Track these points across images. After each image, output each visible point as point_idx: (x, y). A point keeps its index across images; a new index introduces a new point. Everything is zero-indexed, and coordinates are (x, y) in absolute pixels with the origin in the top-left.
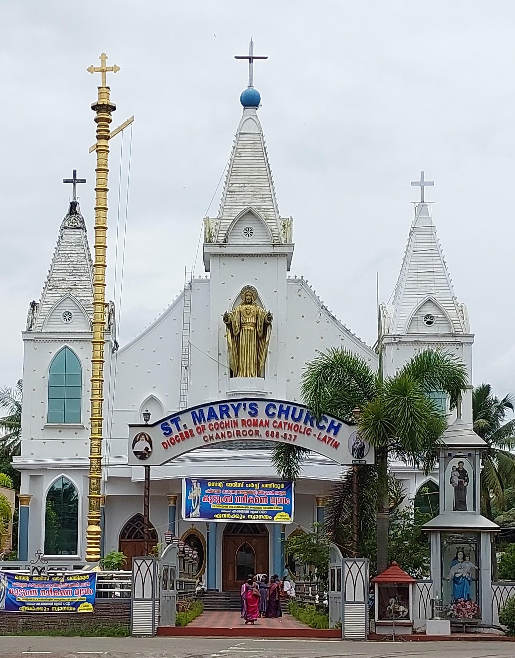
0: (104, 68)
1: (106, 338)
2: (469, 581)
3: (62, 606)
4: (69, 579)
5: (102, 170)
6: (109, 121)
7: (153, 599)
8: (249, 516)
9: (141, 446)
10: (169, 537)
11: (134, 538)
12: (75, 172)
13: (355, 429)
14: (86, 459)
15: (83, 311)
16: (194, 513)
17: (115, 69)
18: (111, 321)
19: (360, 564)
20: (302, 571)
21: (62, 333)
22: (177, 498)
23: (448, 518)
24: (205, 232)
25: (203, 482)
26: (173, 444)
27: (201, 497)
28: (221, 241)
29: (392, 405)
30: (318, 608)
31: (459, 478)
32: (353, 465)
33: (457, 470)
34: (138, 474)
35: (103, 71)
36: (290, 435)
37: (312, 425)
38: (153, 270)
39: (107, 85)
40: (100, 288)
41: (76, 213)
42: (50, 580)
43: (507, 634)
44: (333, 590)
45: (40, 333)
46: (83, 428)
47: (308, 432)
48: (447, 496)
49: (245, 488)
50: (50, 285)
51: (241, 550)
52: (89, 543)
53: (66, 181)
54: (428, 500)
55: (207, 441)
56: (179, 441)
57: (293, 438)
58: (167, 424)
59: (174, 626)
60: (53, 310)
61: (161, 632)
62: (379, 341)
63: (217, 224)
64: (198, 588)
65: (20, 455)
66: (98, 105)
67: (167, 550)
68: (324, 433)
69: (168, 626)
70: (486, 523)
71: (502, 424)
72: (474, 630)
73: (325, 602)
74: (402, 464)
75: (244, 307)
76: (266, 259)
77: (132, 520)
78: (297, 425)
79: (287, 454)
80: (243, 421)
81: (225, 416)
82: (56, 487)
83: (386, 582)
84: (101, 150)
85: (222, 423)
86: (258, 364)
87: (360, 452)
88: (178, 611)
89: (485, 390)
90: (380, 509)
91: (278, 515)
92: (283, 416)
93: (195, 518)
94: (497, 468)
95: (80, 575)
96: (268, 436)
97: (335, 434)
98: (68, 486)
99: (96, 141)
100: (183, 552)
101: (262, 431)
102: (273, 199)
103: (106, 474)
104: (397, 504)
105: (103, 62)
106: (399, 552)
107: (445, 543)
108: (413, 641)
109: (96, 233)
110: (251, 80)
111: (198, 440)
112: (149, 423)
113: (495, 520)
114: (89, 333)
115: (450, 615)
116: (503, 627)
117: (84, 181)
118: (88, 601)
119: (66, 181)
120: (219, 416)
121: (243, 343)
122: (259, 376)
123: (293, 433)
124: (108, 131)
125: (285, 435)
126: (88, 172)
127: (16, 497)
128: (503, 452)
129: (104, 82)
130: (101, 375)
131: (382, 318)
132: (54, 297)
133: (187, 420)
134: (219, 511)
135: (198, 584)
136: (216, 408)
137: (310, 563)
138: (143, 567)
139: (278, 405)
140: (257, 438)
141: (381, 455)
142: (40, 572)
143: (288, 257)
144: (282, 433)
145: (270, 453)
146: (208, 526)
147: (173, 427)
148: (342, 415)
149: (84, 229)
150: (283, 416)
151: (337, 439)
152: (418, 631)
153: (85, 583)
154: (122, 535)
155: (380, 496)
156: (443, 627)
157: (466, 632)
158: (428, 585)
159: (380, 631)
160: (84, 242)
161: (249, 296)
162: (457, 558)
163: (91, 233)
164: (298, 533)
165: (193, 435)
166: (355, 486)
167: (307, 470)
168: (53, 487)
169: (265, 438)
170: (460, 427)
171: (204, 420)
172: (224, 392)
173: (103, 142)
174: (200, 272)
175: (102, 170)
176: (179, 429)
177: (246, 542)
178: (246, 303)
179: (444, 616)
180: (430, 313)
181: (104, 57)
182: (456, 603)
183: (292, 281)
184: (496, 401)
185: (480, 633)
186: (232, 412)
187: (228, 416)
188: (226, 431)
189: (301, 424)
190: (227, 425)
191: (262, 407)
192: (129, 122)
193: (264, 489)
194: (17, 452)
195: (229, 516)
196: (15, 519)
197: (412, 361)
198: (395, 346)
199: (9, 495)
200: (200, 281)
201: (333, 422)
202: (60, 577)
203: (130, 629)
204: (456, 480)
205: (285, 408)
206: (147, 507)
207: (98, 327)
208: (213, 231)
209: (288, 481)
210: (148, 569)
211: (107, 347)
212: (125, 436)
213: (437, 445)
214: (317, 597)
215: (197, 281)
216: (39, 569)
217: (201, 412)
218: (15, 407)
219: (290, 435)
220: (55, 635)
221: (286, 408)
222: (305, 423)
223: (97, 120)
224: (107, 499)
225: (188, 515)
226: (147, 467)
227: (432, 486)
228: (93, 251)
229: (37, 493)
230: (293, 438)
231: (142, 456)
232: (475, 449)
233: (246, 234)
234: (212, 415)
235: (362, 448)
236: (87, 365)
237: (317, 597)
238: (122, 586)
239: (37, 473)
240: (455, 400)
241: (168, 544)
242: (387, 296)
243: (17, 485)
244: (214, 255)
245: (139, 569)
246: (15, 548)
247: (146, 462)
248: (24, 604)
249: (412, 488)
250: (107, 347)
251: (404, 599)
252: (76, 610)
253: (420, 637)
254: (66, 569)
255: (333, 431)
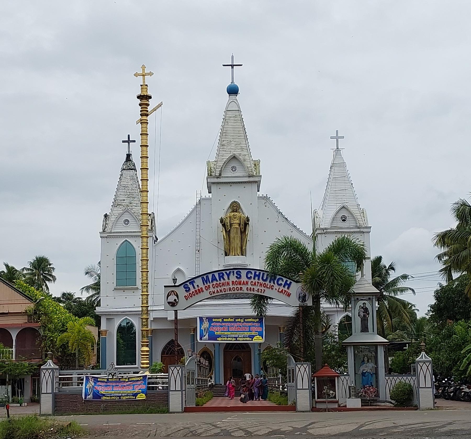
0: (144, 74)
1: (150, 234)
2: (372, 375)
3: (127, 396)
4: (130, 380)
5: (144, 134)
6: (148, 105)
7: (181, 390)
8: (238, 339)
9: (172, 298)
10: (190, 353)
11: (170, 354)
12: (129, 136)
13: (300, 285)
14: (138, 307)
15: (135, 218)
16: (205, 338)
17: (151, 74)
18: (153, 224)
19: (305, 366)
20: (271, 372)
21: (124, 232)
22: (195, 330)
23: (358, 337)
24: (208, 170)
25: (210, 319)
26: (191, 297)
27: (209, 327)
28: (217, 174)
29: (321, 269)
30: (282, 393)
31: (363, 312)
32: (299, 307)
33: (362, 308)
34: (171, 317)
35: (143, 75)
36: (261, 290)
37: (274, 283)
38: (178, 194)
39: (146, 84)
40: (145, 205)
41: (130, 161)
42: (119, 380)
43: (395, 406)
44: (290, 382)
45: (111, 233)
46: (137, 289)
47: (272, 288)
48: (357, 323)
49: (235, 322)
50: (116, 204)
51: (235, 359)
52: (142, 358)
53: (124, 142)
54: (346, 326)
55: (211, 294)
56: (194, 295)
57: (263, 291)
58: (187, 285)
59: (194, 406)
60: (118, 219)
61: (187, 410)
62: (314, 233)
63: (215, 165)
64: (210, 383)
65: (100, 306)
66: (141, 96)
67: (190, 361)
68: (282, 288)
69: (191, 406)
70: (381, 339)
71: (390, 280)
72: (375, 404)
73: (286, 390)
74: (329, 305)
75: (232, 214)
76: (245, 185)
77: (169, 343)
78: (265, 284)
79: (260, 301)
80: (233, 282)
81: (222, 279)
82: (122, 325)
83: (323, 377)
84: (144, 123)
85: (220, 283)
86: (241, 248)
87: (303, 298)
88: (197, 397)
89: (379, 259)
90: (317, 333)
91: (255, 338)
92: (257, 278)
93: (206, 339)
94: (388, 306)
95: (137, 377)
96: (248, 290)
97: (288, 288)
98: (129, 324)
99: (140, 117)
100: (200, 361)
101: (244, 288)
102: (248, 149)
103: (152, 316)
104: (327, 329)
105: (143, 70)
106: (329, 358)
107: (356, 352)
108: (339, 411)
109: (142, 172)
110: (233, 78)
111: (206, 294)
112: (176, 284)
113: (388, 338)
114: (139, 232)
115: (361, 396)
116: (393, 401)
117: (134, 141)
118: (143, 392)
119: (124, 142)
120: (218, 280)
121: (232, 235)
122: (242, 255)
123: (263, 288)
124: (147, 111)
125: (257, 290)
126: (136, 136)
127: (99, 331)
128: (391, 297)
129: (144, 82)
130: (147, 257)
131: (315, 218)
132: (119, 210)
133: (199, 282)
134: (219, 336)
135: (210, 381)
136: (216, 275)
137: (276, 366)
138: (175, 372)
139: (253, 272)
140: (241, 292)
141: (316, 301)
142: (113, 376)
143: (258, 183)
144: (256, 288)
145: (249, 301)
146: (214, 346)
147: (191, 286)
148: (292, 276)
149: (135, 170)
150: (257, 278)
151: (289, 291)
152: (341, 405)
153: (140, 382)
154: (163, 353)
155: (316, 325)
156: (356, 403)
157: (371, 405)
158: (347, 377)
159: (319, 406)
160: (135, 178)
161: (235, 207)
162: (364, 361)
163: (139, 172)
164: (268, 348)
165: (203, 291)
166: (301, 319)
167: (271, 311)
168: (120, 325)
169: (246, 292)
170: (364, 282)
171: (209, 282)
172: (222, 265)
173: (144, 118)
174: (205, 194)
175: (144, 134)
176: (194, 287)
177: (237, 354)
178: (233, 211)
179: (357, 396)
180: (344, 214)
181: (143, 67)
182: (364, 388)
183: (261, 197)
184: (385, 267)
185: (378, 405)
186: (226, 277)
187: (224, 279)
188: (222, 288)
189: (267, 283)
190: (223, 284)
191: (244, 273)
192: (160, 105)
193: (247, 322)
194: (99, 304)
195: (226, 339)
196: (98, 344)
197: (333, 243)
198: (323, 235)
199: (94, 331)
200: (206, 199)
201: (287, 281)
202: (125, 378)
203: (168, 409)
204: (362, 314)
205: (257, 273)
206: (176, 335)
207: (144, 228)
208: (213, 169)
209: (260, 318)
210: (178, 372)
211: (150, 240)
212: (162, 293)
213: (350, 293)
214: (281, 387)
215: (203, 199)
216: (113, 374)
217: (207, 277)
218: (97, 277)
219: (261, 290)
220: (123, 414)
221: (257, 274)
222: (270, 282)
223: (140, 105)
224: (153, 331)
225: (201, 339)
226: (176, 311)
227: (348, 318)
228: (140, 182)
229: (111, 329)
230: (263, 291)
231: (173, 304)
232: (373, 295)
233: (233, 170)
234: (214, 279)
235: (305, 296)
236: (138, 251)
237: (281, 387)
238: (163, 383)
239: (110, 316)
240: (360, 265)
241: (190, 357)
242: (317, 205)
243: (98, 324)
244: (214, 183)
245: (421, 368)
246: (98, 362)
247: (175, 308)
248: (104, 395)
249: (337, 320)
250: (150, 240)
251: (333, 387)
252: (136, 398)
253: (343, 409)
254: (129, 374)
255: (287, 287)
